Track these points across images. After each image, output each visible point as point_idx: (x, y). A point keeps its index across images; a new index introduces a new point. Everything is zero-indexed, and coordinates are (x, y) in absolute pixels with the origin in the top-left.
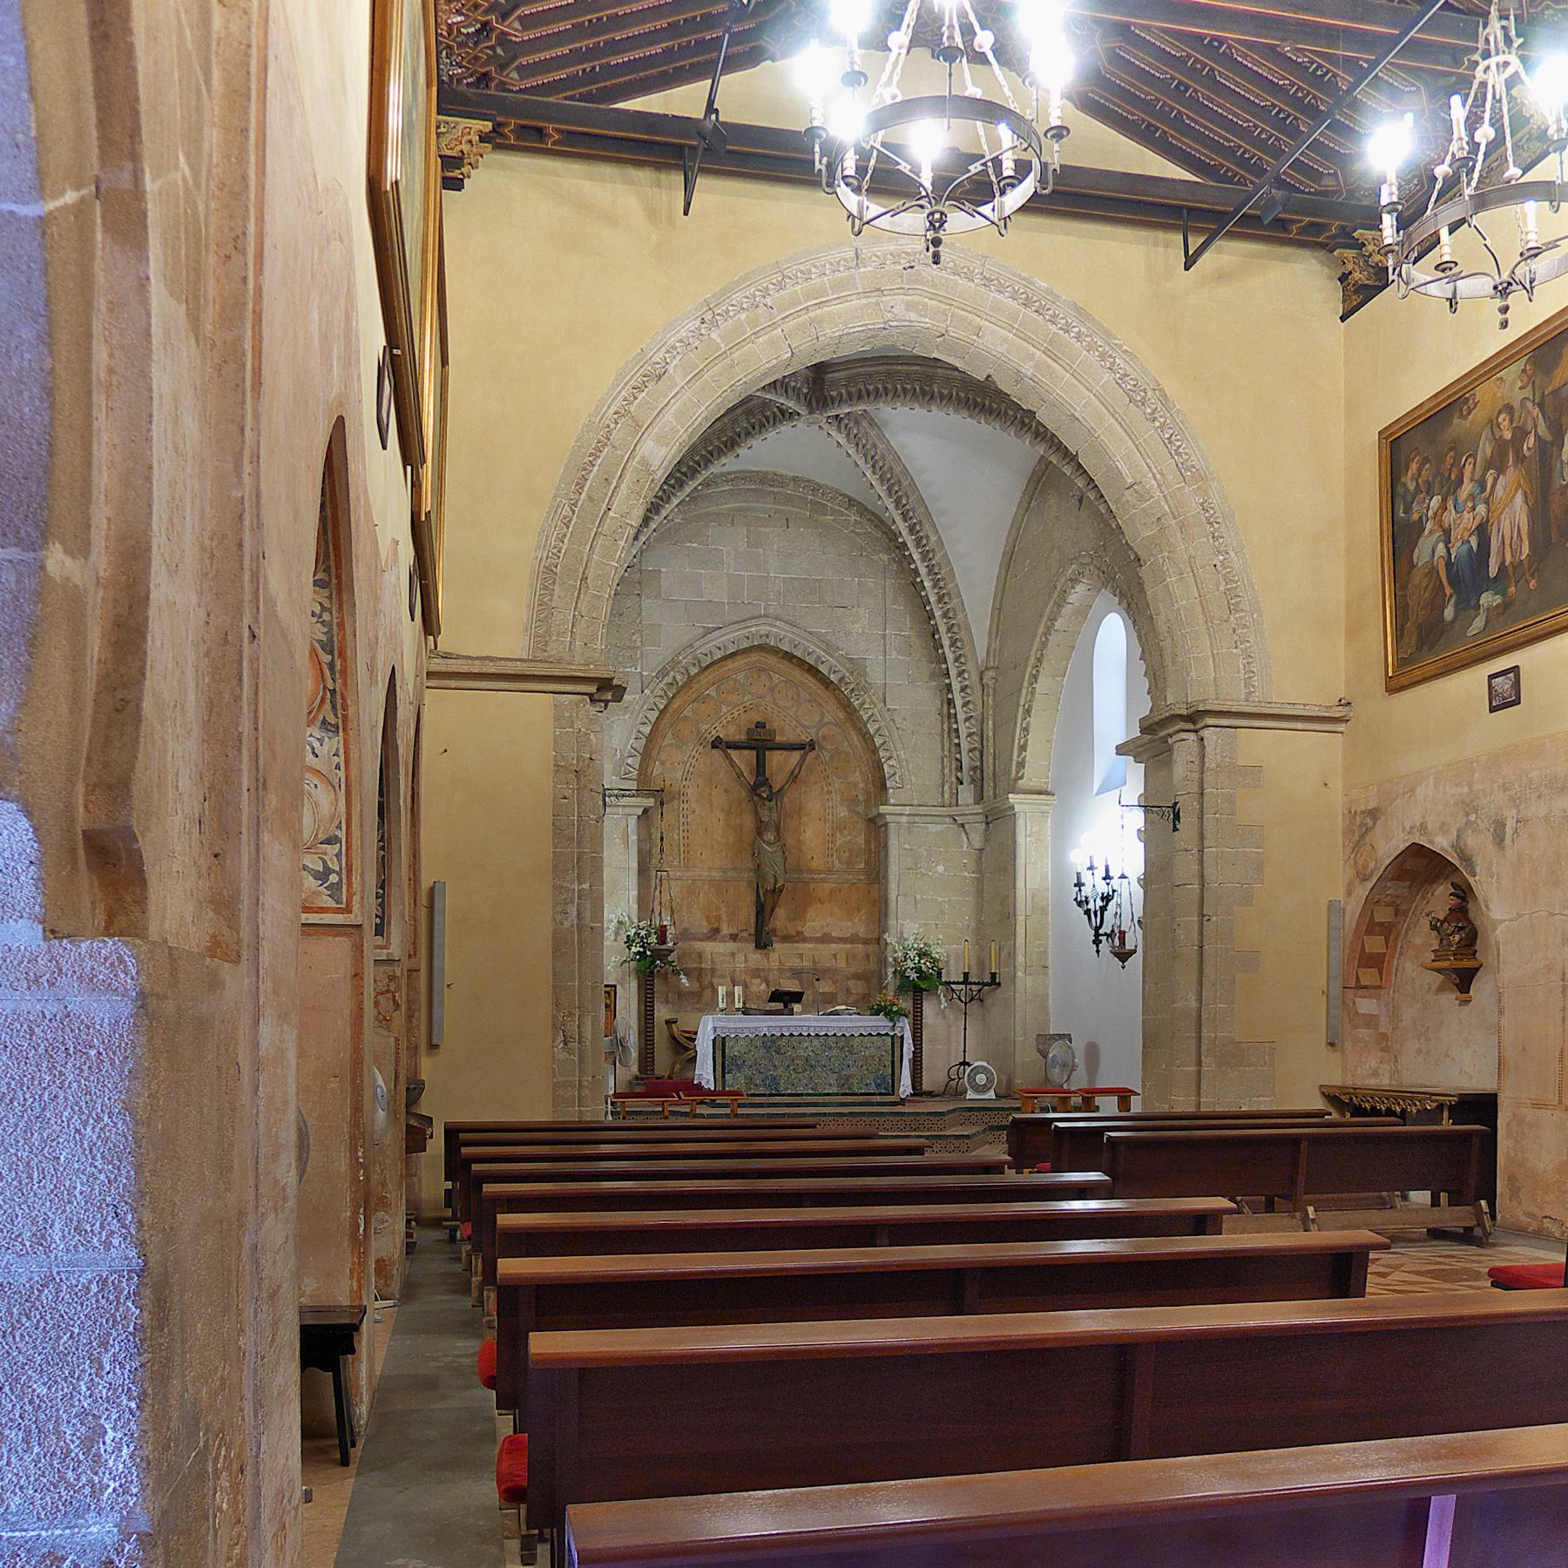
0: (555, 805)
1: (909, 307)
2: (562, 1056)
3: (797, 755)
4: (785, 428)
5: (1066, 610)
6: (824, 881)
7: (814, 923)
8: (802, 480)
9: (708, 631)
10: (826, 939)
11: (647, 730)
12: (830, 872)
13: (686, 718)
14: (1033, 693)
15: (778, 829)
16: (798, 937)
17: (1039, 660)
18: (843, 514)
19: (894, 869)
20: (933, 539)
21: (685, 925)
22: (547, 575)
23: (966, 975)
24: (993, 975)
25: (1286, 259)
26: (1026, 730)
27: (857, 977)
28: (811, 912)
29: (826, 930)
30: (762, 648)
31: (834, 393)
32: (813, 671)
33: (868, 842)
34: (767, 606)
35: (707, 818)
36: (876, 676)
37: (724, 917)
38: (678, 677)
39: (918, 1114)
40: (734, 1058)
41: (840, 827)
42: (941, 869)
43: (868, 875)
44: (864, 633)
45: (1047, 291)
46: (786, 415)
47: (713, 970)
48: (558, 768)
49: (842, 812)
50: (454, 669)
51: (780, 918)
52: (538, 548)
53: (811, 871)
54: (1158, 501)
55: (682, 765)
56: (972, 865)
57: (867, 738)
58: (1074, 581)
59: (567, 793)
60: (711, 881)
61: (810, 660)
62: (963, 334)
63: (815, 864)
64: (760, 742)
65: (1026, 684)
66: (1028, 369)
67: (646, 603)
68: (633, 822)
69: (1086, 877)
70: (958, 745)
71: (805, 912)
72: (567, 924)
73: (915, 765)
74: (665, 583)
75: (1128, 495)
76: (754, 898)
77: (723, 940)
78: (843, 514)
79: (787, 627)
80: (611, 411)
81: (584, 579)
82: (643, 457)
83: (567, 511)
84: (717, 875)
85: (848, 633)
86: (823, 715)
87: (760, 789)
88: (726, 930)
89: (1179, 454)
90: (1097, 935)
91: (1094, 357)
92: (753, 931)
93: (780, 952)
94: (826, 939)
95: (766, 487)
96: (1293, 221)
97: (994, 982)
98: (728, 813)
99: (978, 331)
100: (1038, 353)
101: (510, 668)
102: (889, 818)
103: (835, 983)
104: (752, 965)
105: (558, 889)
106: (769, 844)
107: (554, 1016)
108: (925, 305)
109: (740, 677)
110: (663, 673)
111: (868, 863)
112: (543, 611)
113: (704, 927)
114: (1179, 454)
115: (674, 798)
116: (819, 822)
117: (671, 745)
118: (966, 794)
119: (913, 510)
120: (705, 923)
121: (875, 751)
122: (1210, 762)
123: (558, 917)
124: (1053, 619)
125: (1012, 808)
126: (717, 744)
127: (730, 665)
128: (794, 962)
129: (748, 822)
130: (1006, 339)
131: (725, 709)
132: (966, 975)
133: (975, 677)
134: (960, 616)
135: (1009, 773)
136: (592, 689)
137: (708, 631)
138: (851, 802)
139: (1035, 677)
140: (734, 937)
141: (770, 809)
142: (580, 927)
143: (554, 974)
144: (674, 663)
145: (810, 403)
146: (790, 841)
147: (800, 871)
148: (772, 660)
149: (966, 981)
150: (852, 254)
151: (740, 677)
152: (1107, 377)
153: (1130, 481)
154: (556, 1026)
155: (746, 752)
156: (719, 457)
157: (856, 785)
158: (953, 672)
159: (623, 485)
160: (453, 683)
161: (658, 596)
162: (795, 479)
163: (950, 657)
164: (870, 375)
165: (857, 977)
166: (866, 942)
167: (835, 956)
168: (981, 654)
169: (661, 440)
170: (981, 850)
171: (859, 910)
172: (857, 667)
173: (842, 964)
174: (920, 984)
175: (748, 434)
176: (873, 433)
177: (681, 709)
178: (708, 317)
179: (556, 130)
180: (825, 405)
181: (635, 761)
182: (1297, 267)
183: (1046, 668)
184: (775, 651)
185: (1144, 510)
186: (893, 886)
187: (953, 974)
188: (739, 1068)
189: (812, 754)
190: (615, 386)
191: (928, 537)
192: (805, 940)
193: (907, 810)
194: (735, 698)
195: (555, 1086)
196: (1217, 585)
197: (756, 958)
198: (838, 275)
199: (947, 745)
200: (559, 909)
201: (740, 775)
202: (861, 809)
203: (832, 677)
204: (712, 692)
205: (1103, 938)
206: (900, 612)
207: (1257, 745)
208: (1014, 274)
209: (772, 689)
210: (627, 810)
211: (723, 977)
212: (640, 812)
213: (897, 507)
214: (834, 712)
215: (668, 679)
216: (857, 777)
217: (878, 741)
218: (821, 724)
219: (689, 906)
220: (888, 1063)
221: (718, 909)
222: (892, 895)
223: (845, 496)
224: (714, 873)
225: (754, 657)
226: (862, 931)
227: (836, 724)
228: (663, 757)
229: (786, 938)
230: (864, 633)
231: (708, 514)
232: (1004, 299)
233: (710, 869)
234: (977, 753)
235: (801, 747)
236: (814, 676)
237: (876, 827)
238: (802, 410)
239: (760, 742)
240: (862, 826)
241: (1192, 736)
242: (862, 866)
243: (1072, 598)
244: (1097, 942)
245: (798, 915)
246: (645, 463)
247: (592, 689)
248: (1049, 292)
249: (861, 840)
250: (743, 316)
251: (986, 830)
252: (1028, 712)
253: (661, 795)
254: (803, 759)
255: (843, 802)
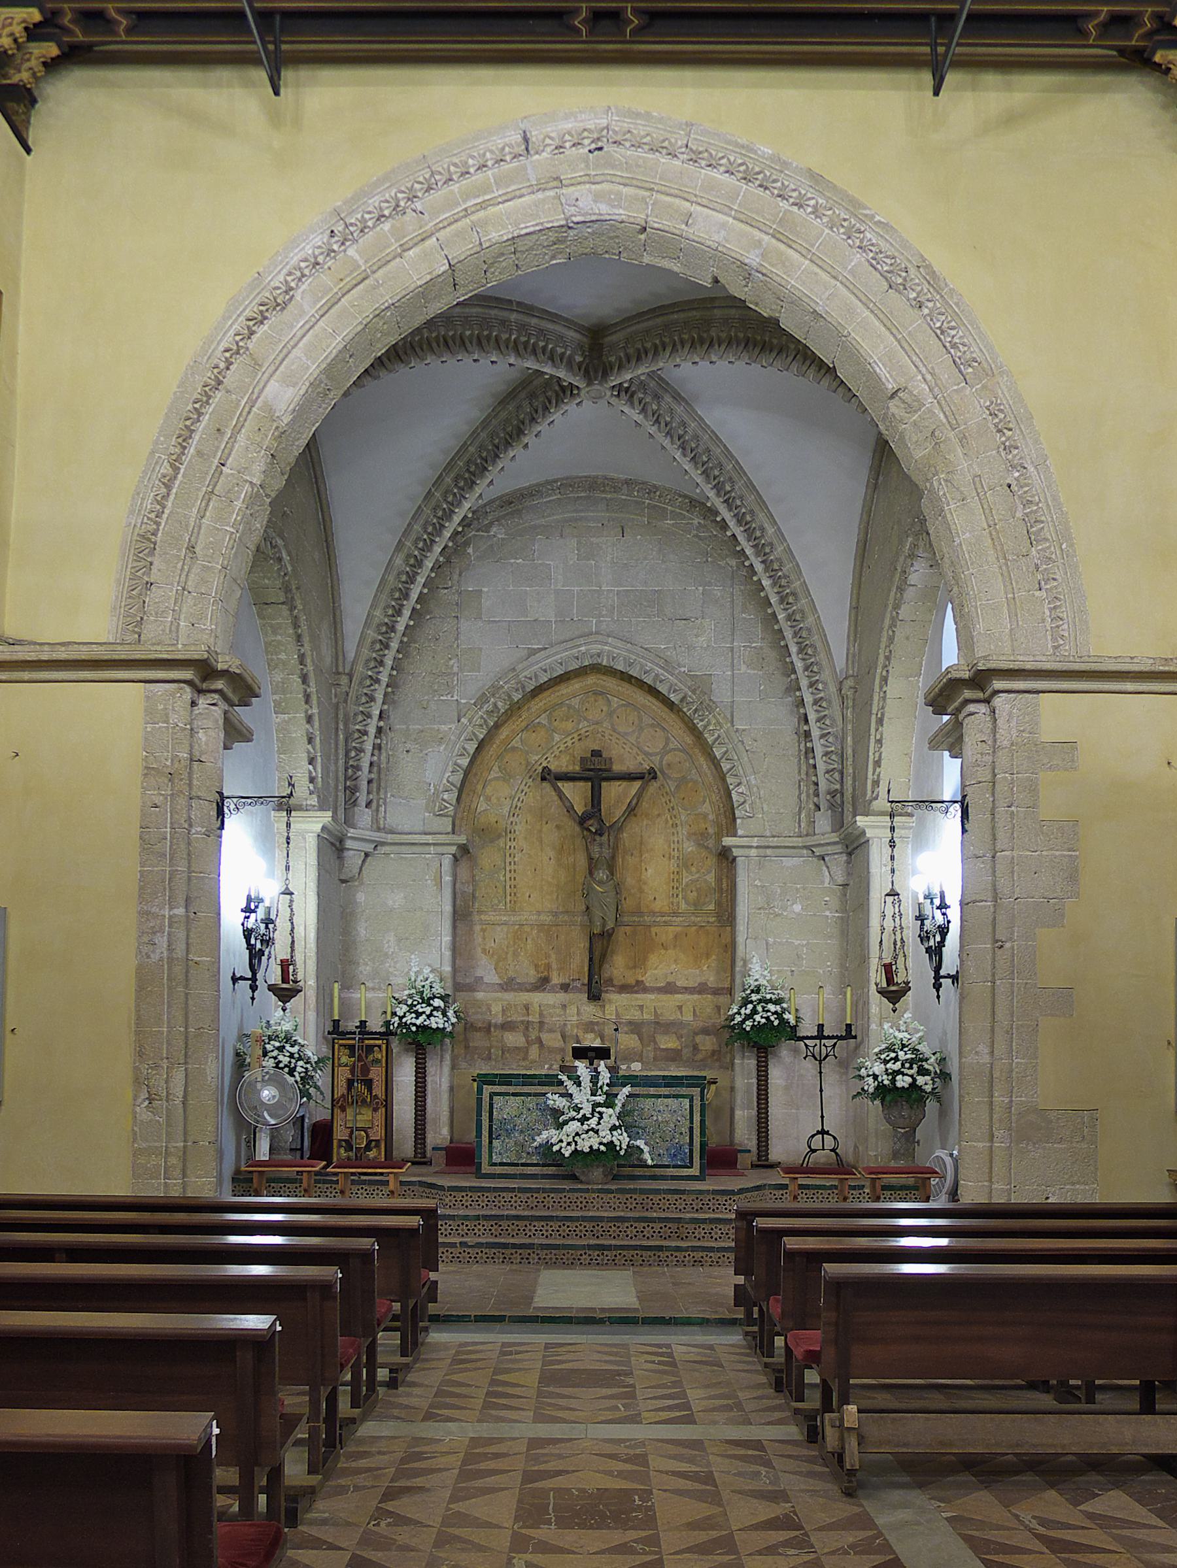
0: (144, 815)
1: (597, 197)
2: (145, 1115)
3: (637, 785)
4: (570, 407)
5: (910, 593)
6: (666, 924)
7: (659, 969)
8: (636, 483)
9: (533, 652)
10: (670, 989)
11: (465, 762)
12: (675, 914)
13: (514, 749)
14: (884, 698)
15: (612, 869)
16: (638, 987)
17: (888, 658)
18: (684, 517)
19: (743, 909)
20: (770, 531)
21: (511, 974)
22: (145, 545)
23: (821, 1027)
24: (849, 1026)
25: (1105, 89)
26: (879, 742)
27: (705, 1031)
28: (653, 959)
29: (670, 979)
30: (596, 669)
31: (613, 359)
32: (653, 691)
33: (719, 880)
34: (599, 622)
35: (535, 867)
36: (721, 694)
37: (554, 966)
38: (500, 704)
39: (701, 1192)
40: (504, 1122)
41: (686, 863)
42: (797, 908)
43: (719, 916)
44: (707, 646)
45: (772, 158)
46: (565, 392)
47: (541, 1023)
48: (148, 771)
49: (689, 847)
50: (21, 656)
51: (618, 967)
52: (132, 512)
53: (653, 913)
54: (930, 411)
55: (507, 797)
56: (835, 903)
57: (715, 763)
58: (912, 556)
59: (158, 800)
60: (541, 926)
61: (649, 680)
62: (666, 224)
63: (657, 906)
64: (595, 772)
65: (877, 688)
66: (753, 258)
67: (464, 625)
68: (447, 861)
69: (928, 911)
70: (815, 766)
71: (645, 959)
72: (155, 957)
73: (768, 794)
74: (486, 603)
75: (894, 407)
76: (587, 945)
77: (553, 990)
78: (684, 517)
79: (620, 644)
80: (221, 348)
81: (191, 548)
82: (265, 403)
83: (166, 469)
84: (546, 919)
85: (691, 648)
86: (667, 739)
87: (592, 822)
88: (556, 980)
89: (954, 346)
90: (937, 977)
91: (839, 236)
92: (586, 981)
93: (617, 1004)
94: (670, 989)
95: (598, 495)
96: (1089, 16)
97: (849, 1033)
98: (560, 851)
99: (687, 218)
100: (766, 238)
101: (84, 654)
102: (735, 852)
103: (680, 1037)
104: (585, 1018)
105: (145, 914)
106: (600, 883)
107: (136, 1069)
108: (619, 194)
109: (575, 702)
110: (482, 700)
111: (719, 904)
112: (139, 585)
113: (532, 976)
114: (954, 346)
115: (499, 836)
116: (660, 863)
117: (496, 779)
118: (823, 822)
119: (741, 498)
120: (532, 972)
121: (723, 779)
122: (1004, 738)
123: (145, 949)
124: (897, 607)
125: (864, 833)
126: (547, 776)
127: (564, 690)
128: (635, 1015)
129: (582, 861)
130: (723, 225)
131: (557, 737)
132: (821, 1027)
133: (833, 689)
134: (811, 619)
135: (865, 794)
136: (188, 675)
137: (533, 652)
138: (700, 837)
139: (885, 680)
140: (565, 987)
141: (601, 845)
142: (171, 960)
143: (138, 1018)
144: (495, 689)
145: (587, 372)
146: (630, 881)
147: (639, 913)
148: (611, 683)
149: (820, 1036)
150: (519, 138)
151: (575, 702)
152: (858, 258)
153: (891, 386)
154: (139, 1081)
155: (581, 784)
156: (506, 451)
157: (705, 816)
158: (804, 683)
159: (241, 438)
160: (26, 675)
161: (479, 617)
162: (627, 482)
163: (799, 665)
164: (647, 331)
165: (705, 1031)
166: (716, 992)
167: (680, 1008)
168: (840, 661)
169: (289, 381)
170: (845, 885)
171: (708, 956)
172: (701, 685)
173: (688, 1017)
174: (766, 1037)
175: (533, 420)
176: (679, 410)
177: (509, 739)
178: (339, 228)
179: (119, 11)
180: (605, 375)
181: (451, 797)
182: (1118, 97)
183: (896, 668)
184: (610, 672)
185: (915, 423)
186: (741, 928)
187: (808, 1028)
188: (509, 1133)
189: (654, 785)
190: (225, 318)
191: (762, 529)
192: (646, 990)
193: (755, 842)
194: (569, 725)
195: (136, 1153)
196: (1012, 511)
197: (590, 1010)
198: (505, 167)
199: (804, 768)
200: (145, 939)
201: (570, 809)
202: (711, 843)
203: (673, 697)
204: (543, 719)
205: (947, 983)
206: (749, 616)
207: (1059, 714)
208: (729, 142)
209: (610, 714)
210: (440, 849)
211: (551, 1031)
212: (453, 849)
213: (718, 495)
214: (679, 735)
215: (488, 707)
216: (706, 808)
217: (725, 766)
218: (665, 751)
219: (516, 954)
220: (685, 1130)
221: (547, 956)
222: (740, 939)
223: (685, 496)
224: (542, 917)
225: (591, 680)
226: (711, 980)
227: (683, 751)
228: (489, 790)
229: (624, 988)
230: (707, 646)
231: (535, 527)
232: (717, 175)
233: (539, 913)
234: (837, 775)
235: (639, 777)
236: (657, 698)
237: (726, 857)
238: (577, 381)
239: (595, 772)
240: (711, 861)
241: (982, 708)
242: (712, 907)
243: (913, 578)
244: (937, 986)
245: (639, 962)
246: (269, 409)
247: (188, 675)
248: (775, 158)
249: (711, 878)
250: (386, 226)
251: (848, 862)
252: (880, 722)
253: (487, 834)
254: (642, 789)
255: (690, 836)
